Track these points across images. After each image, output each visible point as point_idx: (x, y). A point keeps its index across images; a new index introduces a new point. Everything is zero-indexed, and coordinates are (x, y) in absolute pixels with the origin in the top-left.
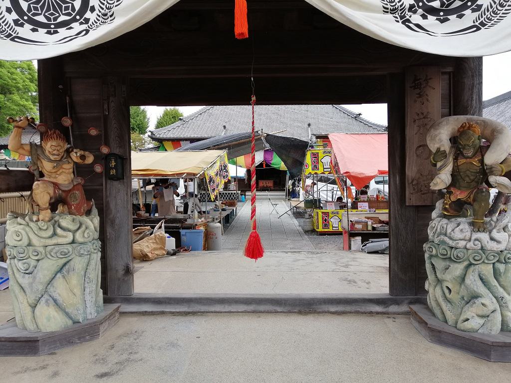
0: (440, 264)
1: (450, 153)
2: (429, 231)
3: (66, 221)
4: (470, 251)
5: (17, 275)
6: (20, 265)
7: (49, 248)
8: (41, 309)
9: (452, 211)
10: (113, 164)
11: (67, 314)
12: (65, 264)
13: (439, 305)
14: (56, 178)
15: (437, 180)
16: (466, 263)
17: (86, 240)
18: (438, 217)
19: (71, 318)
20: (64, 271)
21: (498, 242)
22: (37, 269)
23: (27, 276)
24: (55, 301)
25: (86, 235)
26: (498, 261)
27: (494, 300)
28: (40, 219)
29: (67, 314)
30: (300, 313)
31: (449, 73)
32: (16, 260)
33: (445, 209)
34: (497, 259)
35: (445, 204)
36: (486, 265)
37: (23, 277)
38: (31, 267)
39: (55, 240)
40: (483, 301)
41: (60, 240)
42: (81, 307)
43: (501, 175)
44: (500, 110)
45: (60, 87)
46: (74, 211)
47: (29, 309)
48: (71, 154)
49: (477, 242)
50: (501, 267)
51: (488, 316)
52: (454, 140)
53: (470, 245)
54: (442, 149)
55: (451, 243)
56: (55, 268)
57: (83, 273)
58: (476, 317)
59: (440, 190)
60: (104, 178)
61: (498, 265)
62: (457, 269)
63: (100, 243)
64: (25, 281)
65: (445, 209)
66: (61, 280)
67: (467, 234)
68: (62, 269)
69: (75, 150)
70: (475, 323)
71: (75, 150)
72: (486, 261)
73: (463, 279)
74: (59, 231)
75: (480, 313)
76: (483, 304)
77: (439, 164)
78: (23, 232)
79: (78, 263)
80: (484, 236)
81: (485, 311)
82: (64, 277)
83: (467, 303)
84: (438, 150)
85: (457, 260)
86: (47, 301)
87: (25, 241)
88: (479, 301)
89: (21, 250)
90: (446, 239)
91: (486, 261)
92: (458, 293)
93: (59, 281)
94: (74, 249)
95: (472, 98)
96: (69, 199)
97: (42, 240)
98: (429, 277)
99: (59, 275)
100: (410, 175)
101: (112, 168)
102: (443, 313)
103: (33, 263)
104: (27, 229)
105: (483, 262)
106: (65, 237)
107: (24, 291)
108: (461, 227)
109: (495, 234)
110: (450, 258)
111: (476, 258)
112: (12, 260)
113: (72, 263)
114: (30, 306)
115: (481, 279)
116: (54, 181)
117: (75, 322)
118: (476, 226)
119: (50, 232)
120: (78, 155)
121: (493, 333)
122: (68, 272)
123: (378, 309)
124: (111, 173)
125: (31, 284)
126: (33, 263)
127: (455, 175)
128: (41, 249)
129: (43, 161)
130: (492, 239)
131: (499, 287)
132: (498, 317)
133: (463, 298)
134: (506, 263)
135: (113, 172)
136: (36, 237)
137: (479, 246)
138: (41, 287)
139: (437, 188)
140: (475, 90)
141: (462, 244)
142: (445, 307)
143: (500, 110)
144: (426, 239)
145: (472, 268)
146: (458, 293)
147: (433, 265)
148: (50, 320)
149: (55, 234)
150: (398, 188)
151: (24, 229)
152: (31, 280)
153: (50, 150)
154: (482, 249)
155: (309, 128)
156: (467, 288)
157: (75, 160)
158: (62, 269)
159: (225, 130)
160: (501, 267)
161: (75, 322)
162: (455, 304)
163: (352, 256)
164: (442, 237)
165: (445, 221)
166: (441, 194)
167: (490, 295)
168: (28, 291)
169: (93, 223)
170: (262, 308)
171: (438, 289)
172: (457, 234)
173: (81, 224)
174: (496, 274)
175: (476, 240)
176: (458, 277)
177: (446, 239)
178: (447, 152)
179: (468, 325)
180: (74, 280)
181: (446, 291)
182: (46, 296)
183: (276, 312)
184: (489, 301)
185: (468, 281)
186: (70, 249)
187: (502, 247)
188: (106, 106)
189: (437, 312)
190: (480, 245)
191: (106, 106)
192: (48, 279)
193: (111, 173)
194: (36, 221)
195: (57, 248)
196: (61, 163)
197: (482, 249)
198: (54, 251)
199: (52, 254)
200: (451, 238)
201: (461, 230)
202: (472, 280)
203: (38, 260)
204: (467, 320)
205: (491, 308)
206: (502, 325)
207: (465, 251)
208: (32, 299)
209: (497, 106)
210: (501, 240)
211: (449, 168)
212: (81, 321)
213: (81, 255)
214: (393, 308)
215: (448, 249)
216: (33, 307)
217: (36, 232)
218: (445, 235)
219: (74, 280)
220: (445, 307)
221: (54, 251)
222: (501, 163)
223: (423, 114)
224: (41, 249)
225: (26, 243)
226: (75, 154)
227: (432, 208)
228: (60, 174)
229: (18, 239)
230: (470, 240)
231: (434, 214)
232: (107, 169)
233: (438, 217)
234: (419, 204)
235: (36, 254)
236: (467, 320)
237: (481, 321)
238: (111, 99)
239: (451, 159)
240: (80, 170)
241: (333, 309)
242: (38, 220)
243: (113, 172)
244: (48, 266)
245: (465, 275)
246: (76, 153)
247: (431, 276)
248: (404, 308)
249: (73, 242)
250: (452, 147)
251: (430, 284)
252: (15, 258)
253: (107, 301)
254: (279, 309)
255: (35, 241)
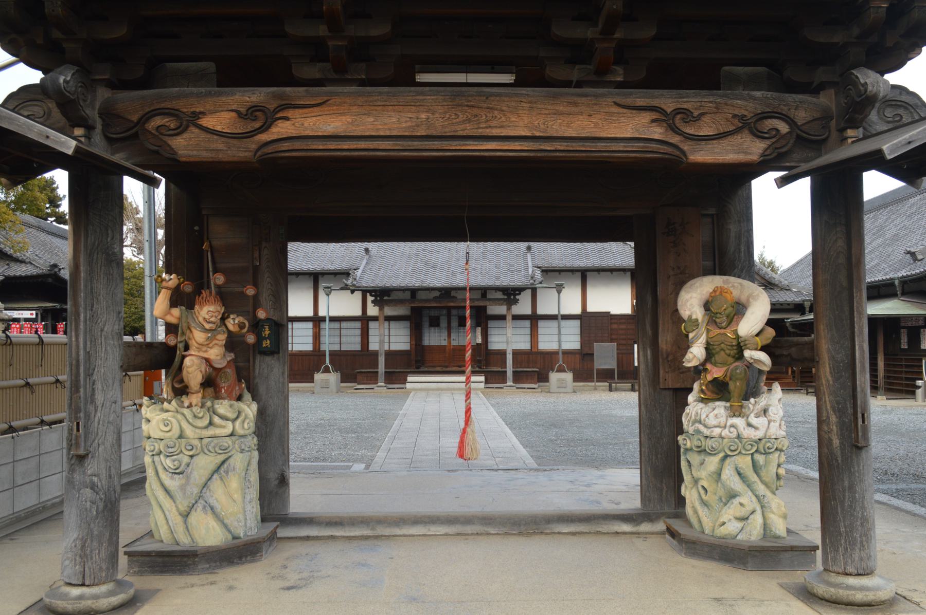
0: (695, 459)
1: (703, 321)
2: (683, 419)
3: (223, 407)
4: (726, 440)
5: (164, 476)
6: (168, 462)
7: (205, 441)
8: (194, 518)
9: (708, 393)
10: (267, 332)
11: (225, 526)
12: (223, 462)
13: (696, 512)
14: (206, 351)
15: (689, 356)
16: (722, 455)
17: (247, 432)
18: (695, 401)
19: (230, 532)
20: (222, 470)
21: (756, 428)
22: (190, 467)
23: (176, 476)
24: (212, 508)
25: (246, 426)
26: (756, 451)
27: (754, 498)
28: (194, 404)
29: (225, 526)
30: (520, 534)
31: (713, 215)
32: (162, 456)
33: (702, 391)
34: (755, 449)
35: (701, 385)
36: (743, 457)
37: (172, 478)
38: (183, 464)
39: (211, 431)
40: (742, 501)
41: (218, 431)
42: (241, 516)
43: (756, 349)
44: (877, 224)
45: (196, 228)
46: (225, 395)
47: (179, 519)
48: (227, 322)
49: (732, 429)
50: (760, 459)
51: (747, 518)
52: (707, 306)
53: (725, 433)
54: (694, 317)
55: (706, 432)
56: (212, 467)
57: (243, 474)
58: (733, 520)
59: (696, 367)
60: (251, 352)
61: (757, 456)
62: (712, 463)
63: (255, 439)
64: (172, 483)
65: (702, 391)
66: (219, 481)
67: (722, 420)
68: (219, 467)
69: (232, 316)
70: (732, 527)
71: (232, 316)
72: (743, 452)
73: (718, 474)
74: (216, 420)
75: (738, 515)
76: (741, 504)
77: (691, 335)
78: (173, 420)
79: (238, 461)
80: (739, 422)
81: (743, 512)
82: (221, 479)
83: (725, 504)
84: (690, 317)
85: (712, 453)
86: (204, 507)
87: (176, 432)
88: (736, 501)
89: (172, 444)
90: (701, 428)
91: (743, 452)
92: (715, 494)
93: (216, 485)
94: (234, 443)
95: (740, 249)
96: (218, 380)
97: (198, 431)
98: (685, 478)
99: (216, 476)
100: (664, 347)
101: (265, 338)
102: (700, 522)
103: (186, 460)
104: (179, 417)
105: (740, 452)
106: (224, 427)
107: (171, 497)
108: (715, 412)
109: (753, 420)
110: (705, 450)
111: (732, 448)
112: (156, 458)
113: (231, 461)
114: (180, 514)
115: (739, 474)
116: (205, 355)
117: (234, 538)
118: (736, 412)
119: (206, 422)
120: (236, 322)
121: (753, 538)
122: (227, 472)
123: (626, 527)
124: (264, 345)
125: (183, 488)
126: (186, 460)
127: (708, 348)
128: (196, 443)
129: (193, 330)
130: (749, 425)
131: (760, 483)
132: (758, 519)
133: (721, 499)
134: (766, 453)
135: (266, 343)
136: (190, 427)
137: (735, 434)
138: (196, 491)
139: (690, 365)
140: (743, 240)
141: (717, 431)
142: (702, 511)
143: (877, 224)
144: (680, 430)
145: (728, 460)
146: (715, 494)
147: (689, 462)
148: (208, 533)
149: (211, 423)
150: (650, 364)
151: (174, 417)
152: (183, 481)
153: (207, 317)
154: (739, 437)
155: (529, 255)
156: (724, 486)
157: (231, 327)
158: (219, 467)
159: (367, 257)
160: (760, 459)
161: (234, 538)
162: (712, 507)
163: (600, 473)
164: (697, 425)
165: (701, 405)
166: (698, 371)
167: (750, 493)
168: (178, 495)
169: (250, 409)
170: (468, 529)
171: (694, 492)
172: (712, 421)
173: (239, 413)
174: (755, 467)
175: (732, 426)
176: (714, 473)
177: (701, 428)
178: (700, 320)
179: (722, 531)
180: (234, 483)
181: (702, 492)
182: (201, 501)
183: (488, 534)
184: (747, 500)
185: (724, 477)
186: (230, 443)
187: (759, 434)
188: (256, 254)
189: (693, 520)
190: (735, 433)
191: (256, 254)
192: (204, 480)
193: (264, 345)
194: (188, 407)
195: (216, 441)
196: (215, 333)
197: (739, 437)
198: (213, 444)
199: (210, 448)
200: (705, 426)
201: (716, 416)
202: (728, 474)
203: (192, 456)
204: (724, 523)
205: (749, 508)
206: (765, 529)
207: (720, 440)
208: (183, 506)
209: (874, 217)
210: (759, 426)
211: (703, 339)
212: (242, 535)
213: (242, 451)
214: (645, 527)
215: (702, 439)
216: (186, 516)
217: (191, 421)
218: (700, 422)
219: (234, 483)
220: (702, 511)
221: (213, 444)
222: (757, 335)
223: (679, 268)
224: (196, 443)
225: (177, 435)
226: (232, 321)
227: (690, 390)
228: (211, 348)
229: (167, 429)
230: (725, 427)
231: (691, 398)
232: (260, 339)
233: (695, 401)
234: (678, 386)
235: (190, 448)
236: (724, 523)
237: (739, 525)
238: (264, 244)
239: (703, 329)
240: (233, 343)
241: (565, 529)
242: (190, 406)
243: (266, 343)
244: (205, 463)
245: (721, 470)
246: (234, 319)
247: (687, 477)
248: (660, 526)
249: (232, 435)
250: (705, 315)
251: (686, 487)
252: (160, 453)
253: (264, 519)
254: (492, 530)
255: (189, 431)
